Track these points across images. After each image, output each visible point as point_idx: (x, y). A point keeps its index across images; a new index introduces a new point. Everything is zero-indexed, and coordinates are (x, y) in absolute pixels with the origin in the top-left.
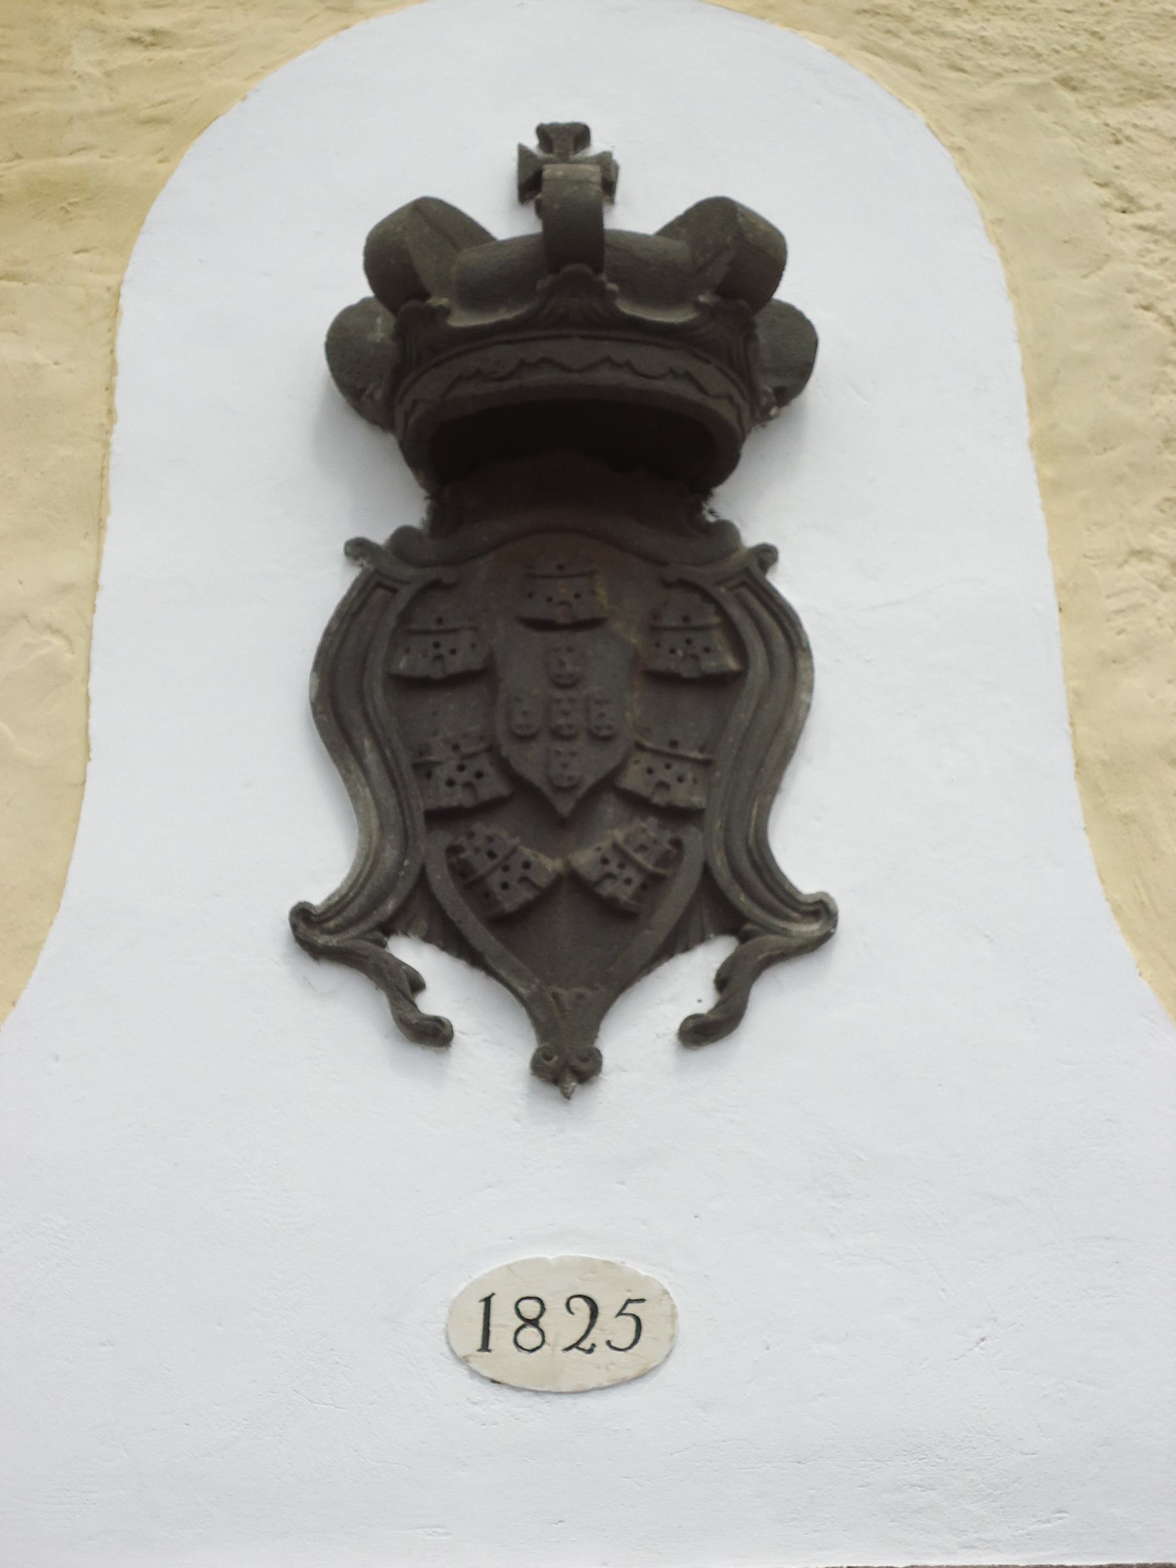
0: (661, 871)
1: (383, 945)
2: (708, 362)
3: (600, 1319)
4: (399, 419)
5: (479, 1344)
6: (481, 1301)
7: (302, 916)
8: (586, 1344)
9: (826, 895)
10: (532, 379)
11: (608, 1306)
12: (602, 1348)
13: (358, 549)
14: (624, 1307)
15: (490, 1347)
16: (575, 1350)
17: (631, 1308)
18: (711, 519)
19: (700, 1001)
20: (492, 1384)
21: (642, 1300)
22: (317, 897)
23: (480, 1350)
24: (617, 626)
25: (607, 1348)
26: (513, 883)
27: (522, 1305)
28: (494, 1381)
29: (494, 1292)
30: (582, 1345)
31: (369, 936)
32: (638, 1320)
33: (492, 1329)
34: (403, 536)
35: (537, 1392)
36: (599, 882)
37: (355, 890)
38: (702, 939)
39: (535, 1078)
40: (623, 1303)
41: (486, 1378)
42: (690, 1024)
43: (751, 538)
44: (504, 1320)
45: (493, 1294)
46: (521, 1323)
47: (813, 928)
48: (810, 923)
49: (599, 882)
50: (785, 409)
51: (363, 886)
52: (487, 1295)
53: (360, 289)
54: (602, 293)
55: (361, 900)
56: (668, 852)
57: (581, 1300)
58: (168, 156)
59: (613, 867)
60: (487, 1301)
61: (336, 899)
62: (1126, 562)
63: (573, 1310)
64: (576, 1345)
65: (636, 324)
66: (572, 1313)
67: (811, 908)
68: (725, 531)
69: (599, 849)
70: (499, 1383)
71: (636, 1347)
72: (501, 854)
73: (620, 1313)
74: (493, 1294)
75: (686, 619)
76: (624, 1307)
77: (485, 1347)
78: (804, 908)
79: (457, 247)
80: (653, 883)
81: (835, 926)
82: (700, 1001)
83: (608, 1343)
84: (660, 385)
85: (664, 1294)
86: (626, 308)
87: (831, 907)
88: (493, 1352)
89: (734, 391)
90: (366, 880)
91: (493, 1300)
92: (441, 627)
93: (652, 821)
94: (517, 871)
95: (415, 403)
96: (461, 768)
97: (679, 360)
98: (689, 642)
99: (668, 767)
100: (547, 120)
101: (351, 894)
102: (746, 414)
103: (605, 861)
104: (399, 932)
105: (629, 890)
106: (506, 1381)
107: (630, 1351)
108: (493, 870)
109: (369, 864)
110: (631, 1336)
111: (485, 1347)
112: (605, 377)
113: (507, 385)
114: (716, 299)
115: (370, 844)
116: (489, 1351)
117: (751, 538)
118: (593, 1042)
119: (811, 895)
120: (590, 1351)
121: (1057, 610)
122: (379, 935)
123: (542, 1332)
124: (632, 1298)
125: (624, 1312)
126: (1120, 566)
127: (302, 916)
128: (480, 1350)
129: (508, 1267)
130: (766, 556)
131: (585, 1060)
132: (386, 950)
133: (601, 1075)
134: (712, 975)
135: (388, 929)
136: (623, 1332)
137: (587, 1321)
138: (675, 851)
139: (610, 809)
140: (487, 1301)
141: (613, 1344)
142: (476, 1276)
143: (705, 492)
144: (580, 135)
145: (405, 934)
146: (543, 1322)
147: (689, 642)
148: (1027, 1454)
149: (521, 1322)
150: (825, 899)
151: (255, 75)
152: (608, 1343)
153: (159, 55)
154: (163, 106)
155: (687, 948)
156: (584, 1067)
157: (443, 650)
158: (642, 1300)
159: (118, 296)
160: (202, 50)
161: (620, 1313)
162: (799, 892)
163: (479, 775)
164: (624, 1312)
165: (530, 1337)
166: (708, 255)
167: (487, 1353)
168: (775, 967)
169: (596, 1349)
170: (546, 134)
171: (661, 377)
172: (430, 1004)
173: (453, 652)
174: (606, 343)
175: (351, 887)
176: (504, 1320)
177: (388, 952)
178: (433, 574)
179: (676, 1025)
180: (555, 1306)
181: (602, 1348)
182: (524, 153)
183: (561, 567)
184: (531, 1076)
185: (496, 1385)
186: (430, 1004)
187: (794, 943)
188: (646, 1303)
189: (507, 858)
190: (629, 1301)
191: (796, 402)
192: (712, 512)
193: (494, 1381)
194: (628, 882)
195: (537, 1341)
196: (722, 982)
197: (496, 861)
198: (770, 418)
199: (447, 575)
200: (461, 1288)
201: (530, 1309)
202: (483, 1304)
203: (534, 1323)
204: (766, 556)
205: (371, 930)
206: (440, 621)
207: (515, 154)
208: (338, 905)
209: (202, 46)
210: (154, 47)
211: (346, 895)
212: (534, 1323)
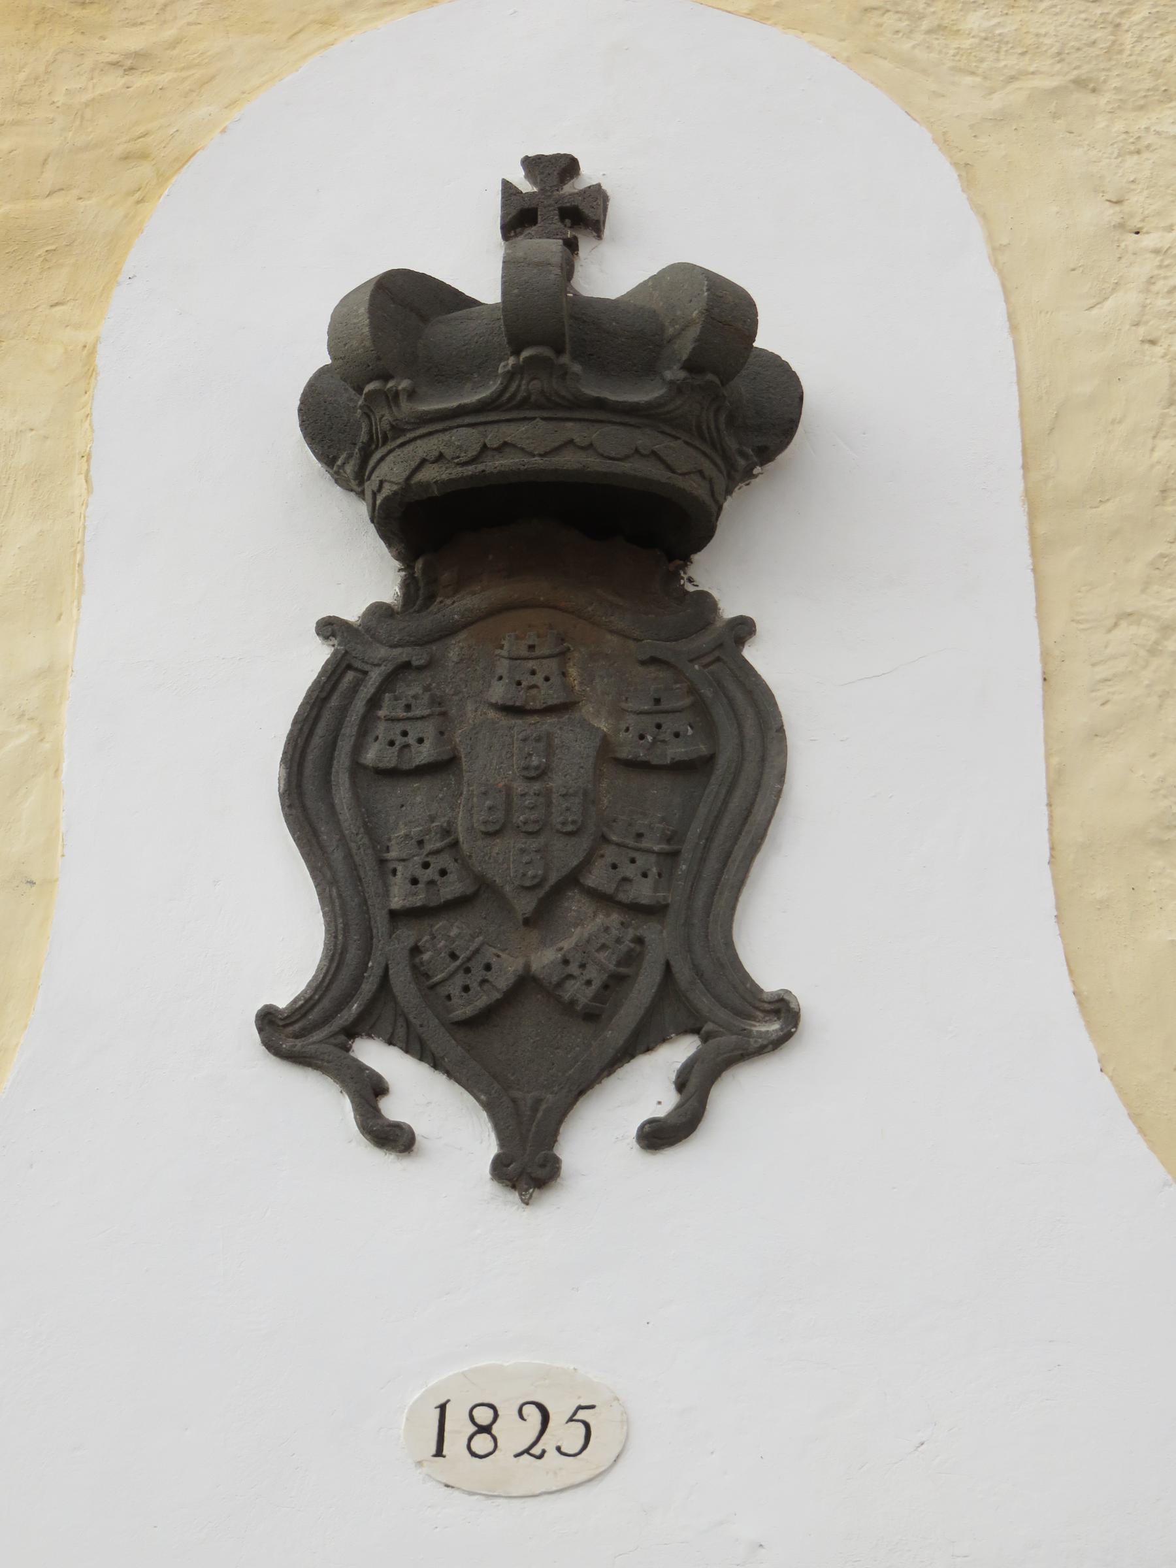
0: (623, 970)
2: (677, 438)
3: (551, 1424)
4: (368, 494)
5: (433, 1450)
6: (436, 1408)
7: (268, 1020)
8: (536, 1450)
9: (787, 992)
12: (552, 1453)
13: (329, 628)
14: (575, 1413)
15: (444, 1453)
16: (526, 1456)
17: (581, 1415)
18: (690, 588)
19: (659, 1103)
20: (446, 1488)
21: (593, 1407)
22: (282, 1001)
23: (435, 1456)
24: (587, 710)
25: (557, 1453)
26: (474, 986)
27: (475, 1412)
28: (447, 1486)
29: (449, 1398)
30: (533, 1451)
31: (332, 1040)
32: (587, 1426)
33: (446, 1434)
34: (379, 612)
35: (488, 1496)
36: (560, 984)
37: (320, 993)
38: (664, 1040)
40: (574, 1409)
41: (440, 1482)
42: (647, 1128)
43: (729, 609)
44: (458, 1428)
45: (448, 1401)
46: (474, 1429)
47: (773, 1027)
49: (560, 984)
50: (770, 466)
51: (328, 988)
52: (442, 1401)
54: (564, 373)
55: (326, 1003)
56: (631, 951)
57: (533, 1407)
58: (142, 196)
60: (443, 1408)
61: (301, 1002)
62: (1116, 625)
63: (525, 1417)
64: (527, 1451)
65: (600, 404)
68: (705, 603)
69: (561, 949)
70: (453, 1487)
72: (463, 956)
73: (571, 1420)
74: (448, 1401)
75: (657, 701)
76: (575, 1413)
77: (439, 1453)
78: (766, 1006)
79: (425, 319)
80: (616, 983)
81: (796, 1025)
82: (659, 1103)
83: (559, 1449)
84: (626, 467)
86: (592, 390)
88: (447, 1457)
89: (707, 466)
90: (331, 982)
91: (448, 1406)
92: (410, 714)
93: (615, 918)
95: (381, 483)
97: (644, 439)
100: (532, 153)
102: (720, 483)
103: (566, 962)
105: (590, 991)
106: (457, 1486)
107: (579, 1457)
108: (452, 975)
109: (335, 965)
110: (581, 1442)
111: (439, 1453)
112: (569, 460)
113: (470, 470)
115: (335, 945)
116: (444, 1457)
117: (729, 609)
118: (552, 1150)
119: (772, 993)
120: (540, 1457)
121: (1040, 681)
122: (342, 1038)
123: (495, 1439)
124: (583, 1404)
125: (575, 1418)
126: (1109, 631)
127: (268, 1020)
128: (435, 1456)
129: (464, 1374)
130: (744, 629)
131: (543, 1166)
132: (351, 1054)
133: (559, 1180)
134: (673, 1077)
135: (352, 1032)
136: (572, 1437)
137: (538, 1427)
138: (638, 948)
139: (575, 904)
140: (443, 1408)
141: (563, 1450)
142: (432, 1383)
143: (686, 559)
144: (568, 167)
145: (369, 1036)
146: (495, 1429)
147: (659, 726)
148: (959, 1557)
150: (786, 997)
152: (559, 1449)
155: (648, 1049)
156: (540, 1173)
157: (411, 740)
158: (593, 1407)
159: (93, 352)
160: (184, 74)
161: (571, 1420)
162: (762, 991)
163: (443, 873)
165: (482, 1443)
168: (729, 1070)
169: (546, 1455)
170: (532, 165)
172: (393, 1109)
173: (421, 741)
174: (569, 425)
175: (331, 960)
176: (458, 1428)
178: (401, 654)
179: (634, 1132)
180: (508, 1413)
181: (552, 1453)
182: (508, 189)
183: (531, 648)
184: (492, 1182)
186: (393, 1109)
188: (596, 1408)
189: (469, 959)
190: (580, 1408)
191: (781, 458)
192: (690, 580)
193: (447, 1486)
197: (458, 963)
199: (418, 657)
200: (417, 1396)
201: (483, 1415)
202: (438, 1410)
203: (486, 1429)
204: (744, 629)
206: (408, 707)
208: (304, 1007)
209: (183, 69)
210: (133, 71)
211: (311, 998)
212: (486, 1429)
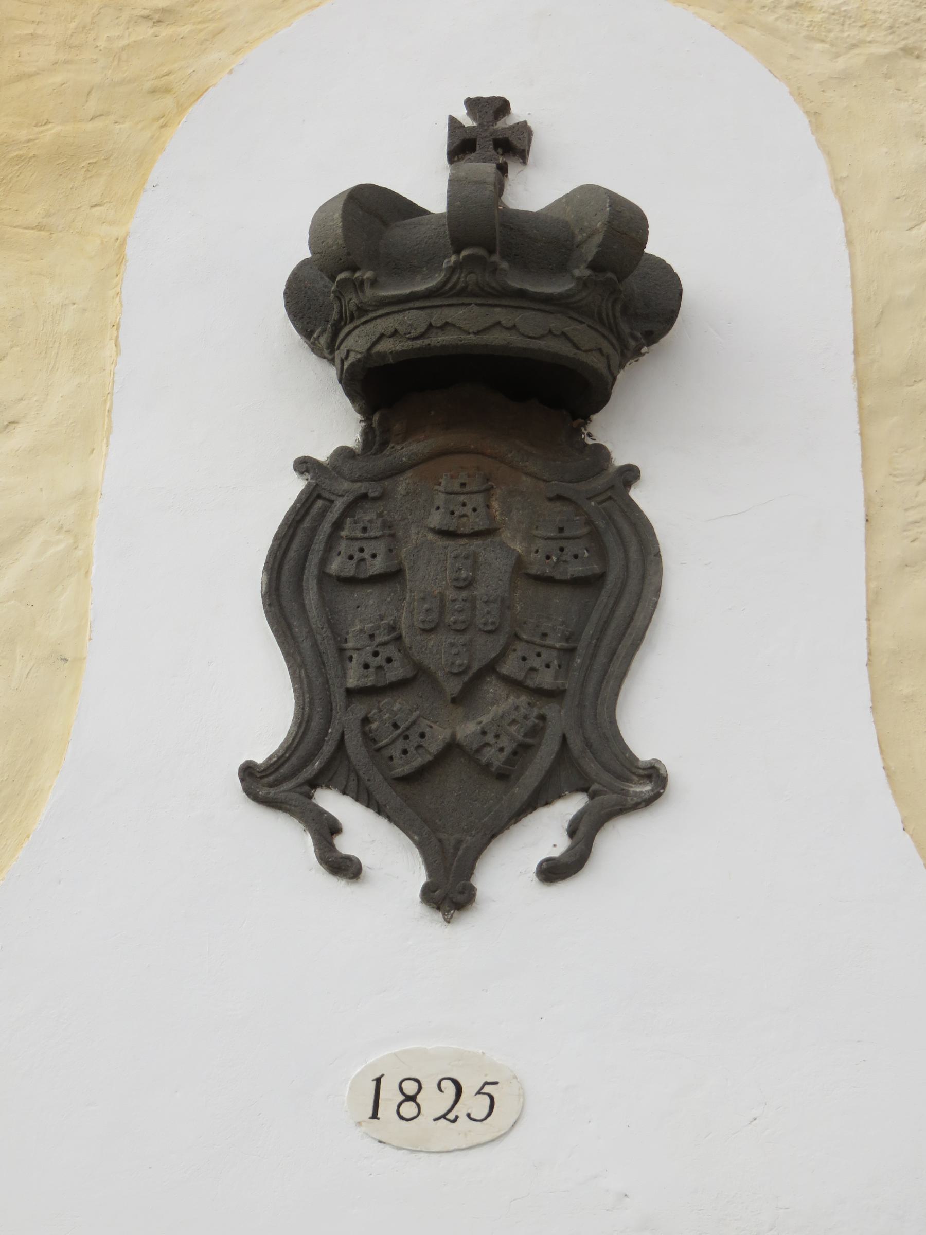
1: (311, 797)
5: (370, 1113)
6: (373, 1080)
8: (451, 1116)
9: (658, 761)
10: (439, 339)
11: (469, 1088)
12: (463, 1118)
14: (482, 1088)
16: (443, 1120)
17: (487, 1089)
18: (589, 442)
19: (555, 846)
20: (379, 1144)
21: (496, 1083)
22: (260, 758)
23: (370, 1118)
24: (506, 535)
26: (411, 750)
28: (380, 1142)
30: (448, 1117)
31: (298, 790)
32: (492, 1099)
34: (343, 454)
36: (478, 750)
38: (559, 796)
39: (424, 905)
42: (544, 866)
43: (620, 459)
45: (383, 1075)
47: (646, 788)
48: (644, 784)
52: (378, 1075)
53: (308, 254)
54: (495, 269)
56: (535, 725)
58: (165, 122)
59: (490, 738)
60: (378, 1081)
61: (275, 759)
64: (444, 1116)
65: (522, 294)
66: (476, 1095)
67: (646, 772)
68: (601, 453)
71: (489, 1118)
72: (403, 726)
73: (479, 1093)
74: (383, 1075)
76: (482, 1088)
77: (375, 1116)
78: (641, 772)
79: (385, 224)
80: (523, 750)
81: (664, 788)
82: (555, 846)
83: (469, 1115)
84: (541, 344)
85: (513, 1078)
86: (516, 283)
87: (662, 772)
92: (366, 535)
94: (415, 740)
96: (376, 654)
97: (556, 322)
98: (562, 549)
99: (539, 655)
101: (287, 755)
103: (484, 733)
104: (323, 785)
105: (503, 757)
107: (484, 1122)
111: (375, 1116)
112: (497, 338)
113: (419, 343)
114: (588, 272)
115: (303, 715)
116: (378, 1119)
117: (620, 459)
119: (646, 762)
120: (454, 1121)
121: (864, 522)
123: (419, 1106)
124: (489, 1081)
125: (483, 1091)
128: (370, 1118)
129: (395, 1054)
130: (630, 474)
132: (313, 801)
133: (474, 904)
134: (566, 825)
135: (314, 784)
136: (480, 1106)
138: (541, 724)
139: (492, 688)
140: (378, 1081)
141: (472, 1116)
142: (370, 1061)
144: (501, 107)
145: (328, 787)
146: (419, 1098)
147: (562, 549)
148: (781, 1208)
149: (402, 1098)
151: (237, 51)
152: (469, 1115)
153: (165, 32)
154: (166, 77)
155: (547, 803)
156: (460, 898)
158: (496, 1083)
160: (200, 27)
161: (479, 1093)
163: (389, 660)
164: (483, 1091)
165: (409, 1109)
166: (585, 235)
167: (376, 1120)
170: (474, 105)
171: (541, 337)
172: (345, 845)
173: (374, 556)
174: (498, 310)
177: (316, 802)
178: (361, 488)
179: (534, 868)
180: (429, 1086)
181: (463, 1118)
182: (454, 123)
183: (463, 485)
184: (421, 904)
185: (382, 1144)
186: (345, 845)
187: (630, 801)
189: (408, 729)
190: (487, 1083)
192: (589, 435)
194: (501, 750)
195: (415, 1111)
196: (572, 832)
197: (399, 731)
198: (643, 354)
201: (410, 1088)
202: (375, 1082)
203: (412, 1098)
204: (630, 474)
205: (300, 785)
206: (365, 529)
207: (447, 122)
210: (160, 23)
211: (283, 756)
212: (412, 1098)
